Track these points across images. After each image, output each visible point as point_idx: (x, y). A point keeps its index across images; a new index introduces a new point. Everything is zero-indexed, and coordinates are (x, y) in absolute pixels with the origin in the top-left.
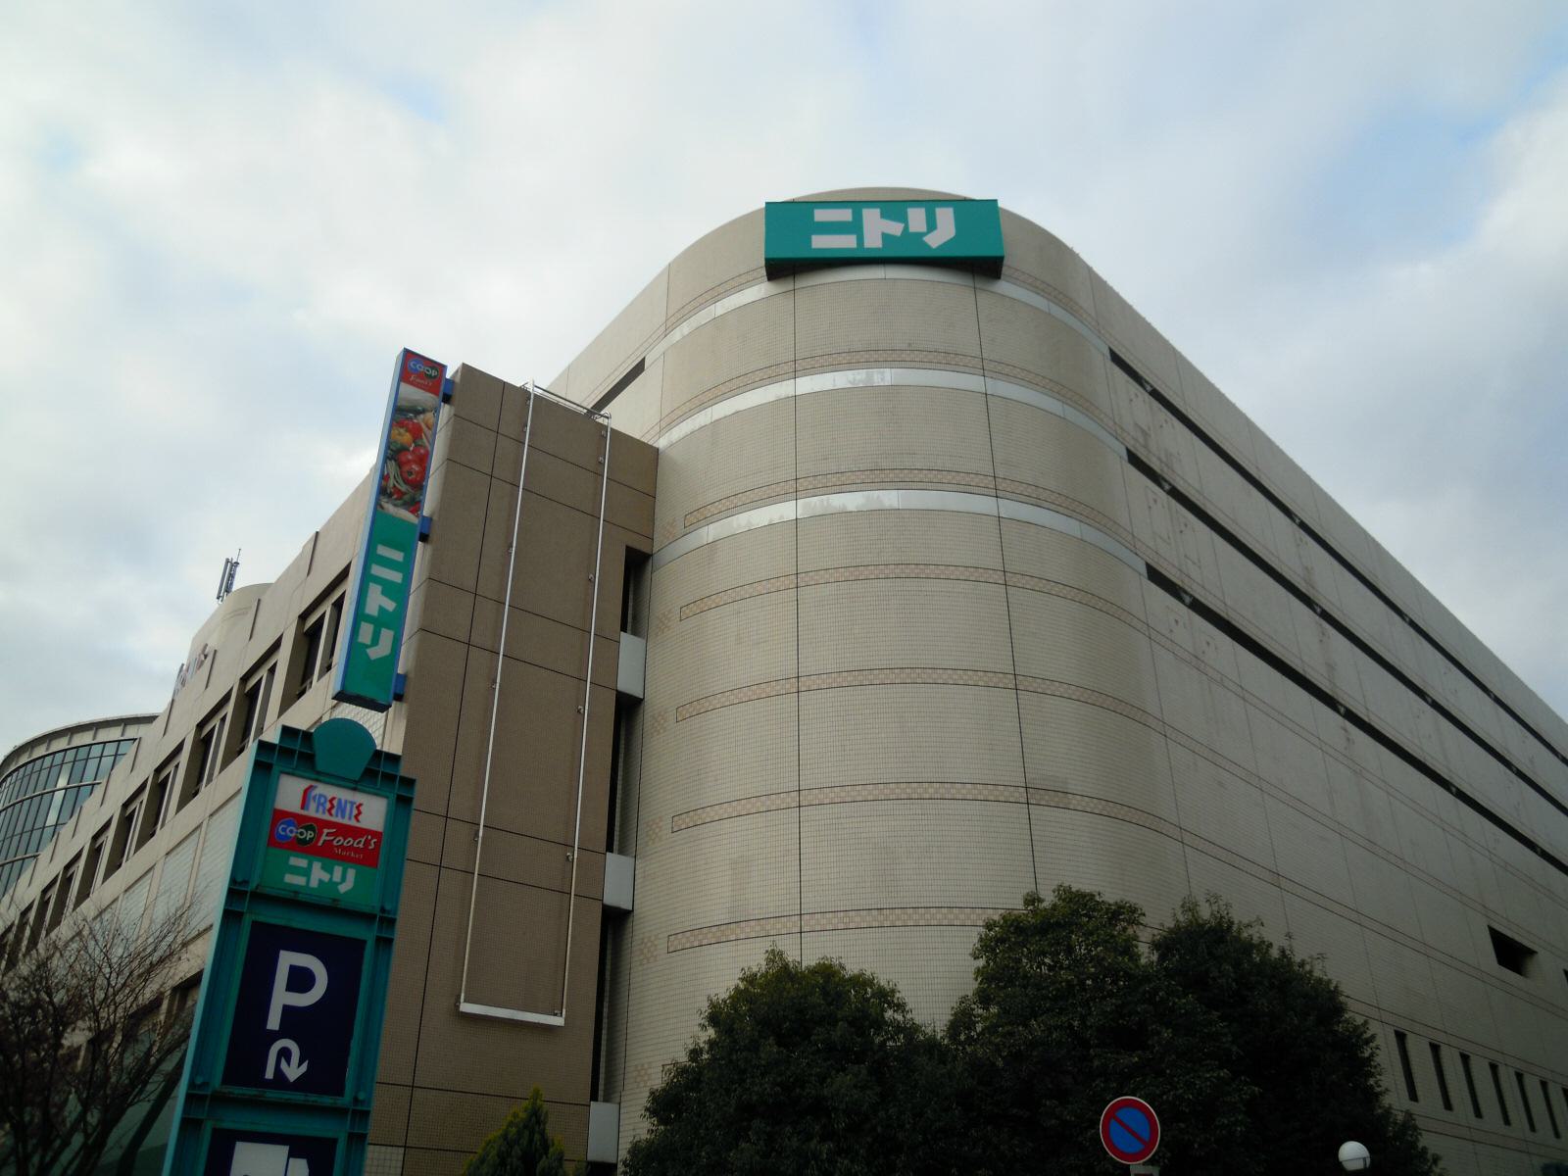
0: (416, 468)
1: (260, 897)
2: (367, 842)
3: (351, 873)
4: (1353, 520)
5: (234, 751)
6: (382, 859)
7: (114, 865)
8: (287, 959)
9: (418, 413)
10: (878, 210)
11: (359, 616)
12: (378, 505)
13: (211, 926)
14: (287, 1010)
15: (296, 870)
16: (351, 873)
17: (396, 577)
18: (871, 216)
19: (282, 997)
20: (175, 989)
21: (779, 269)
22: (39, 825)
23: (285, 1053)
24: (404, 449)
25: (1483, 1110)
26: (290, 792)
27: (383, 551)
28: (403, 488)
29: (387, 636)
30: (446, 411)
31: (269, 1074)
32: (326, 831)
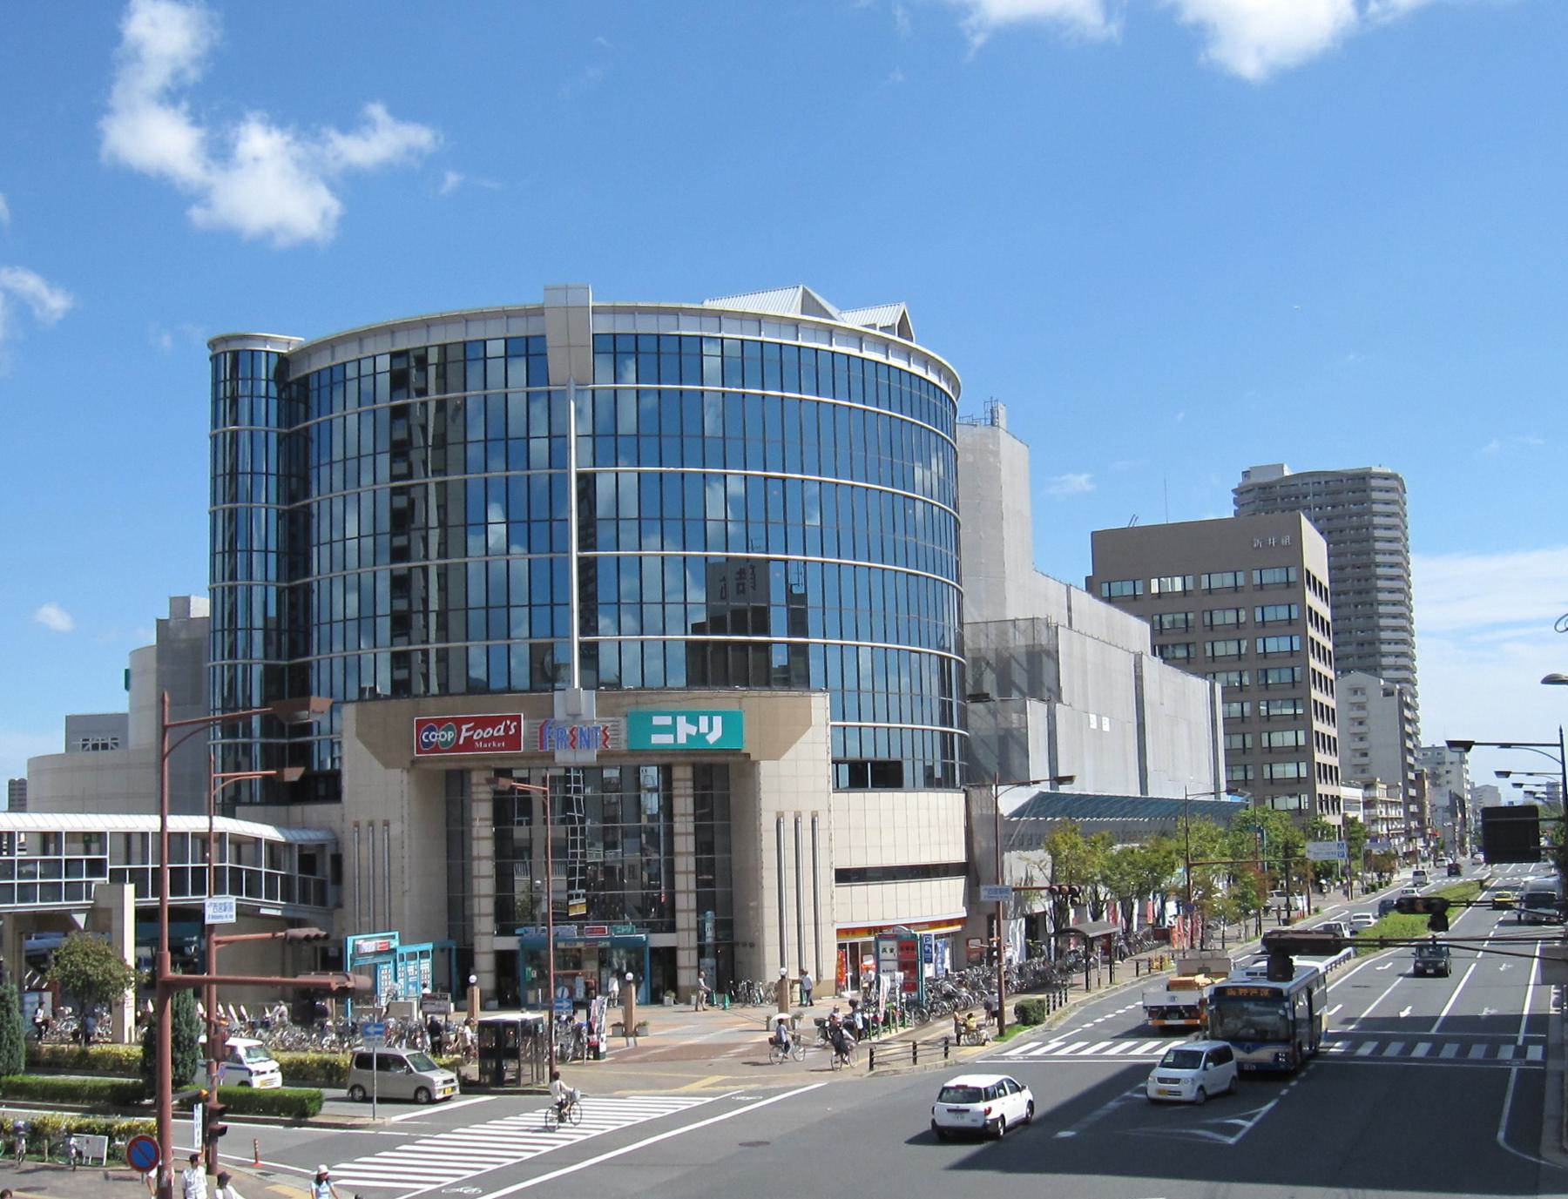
2: (507, 728)
3: (717, 721)
15: (662, 730)
25: (859, 890)
32: (464, 728)
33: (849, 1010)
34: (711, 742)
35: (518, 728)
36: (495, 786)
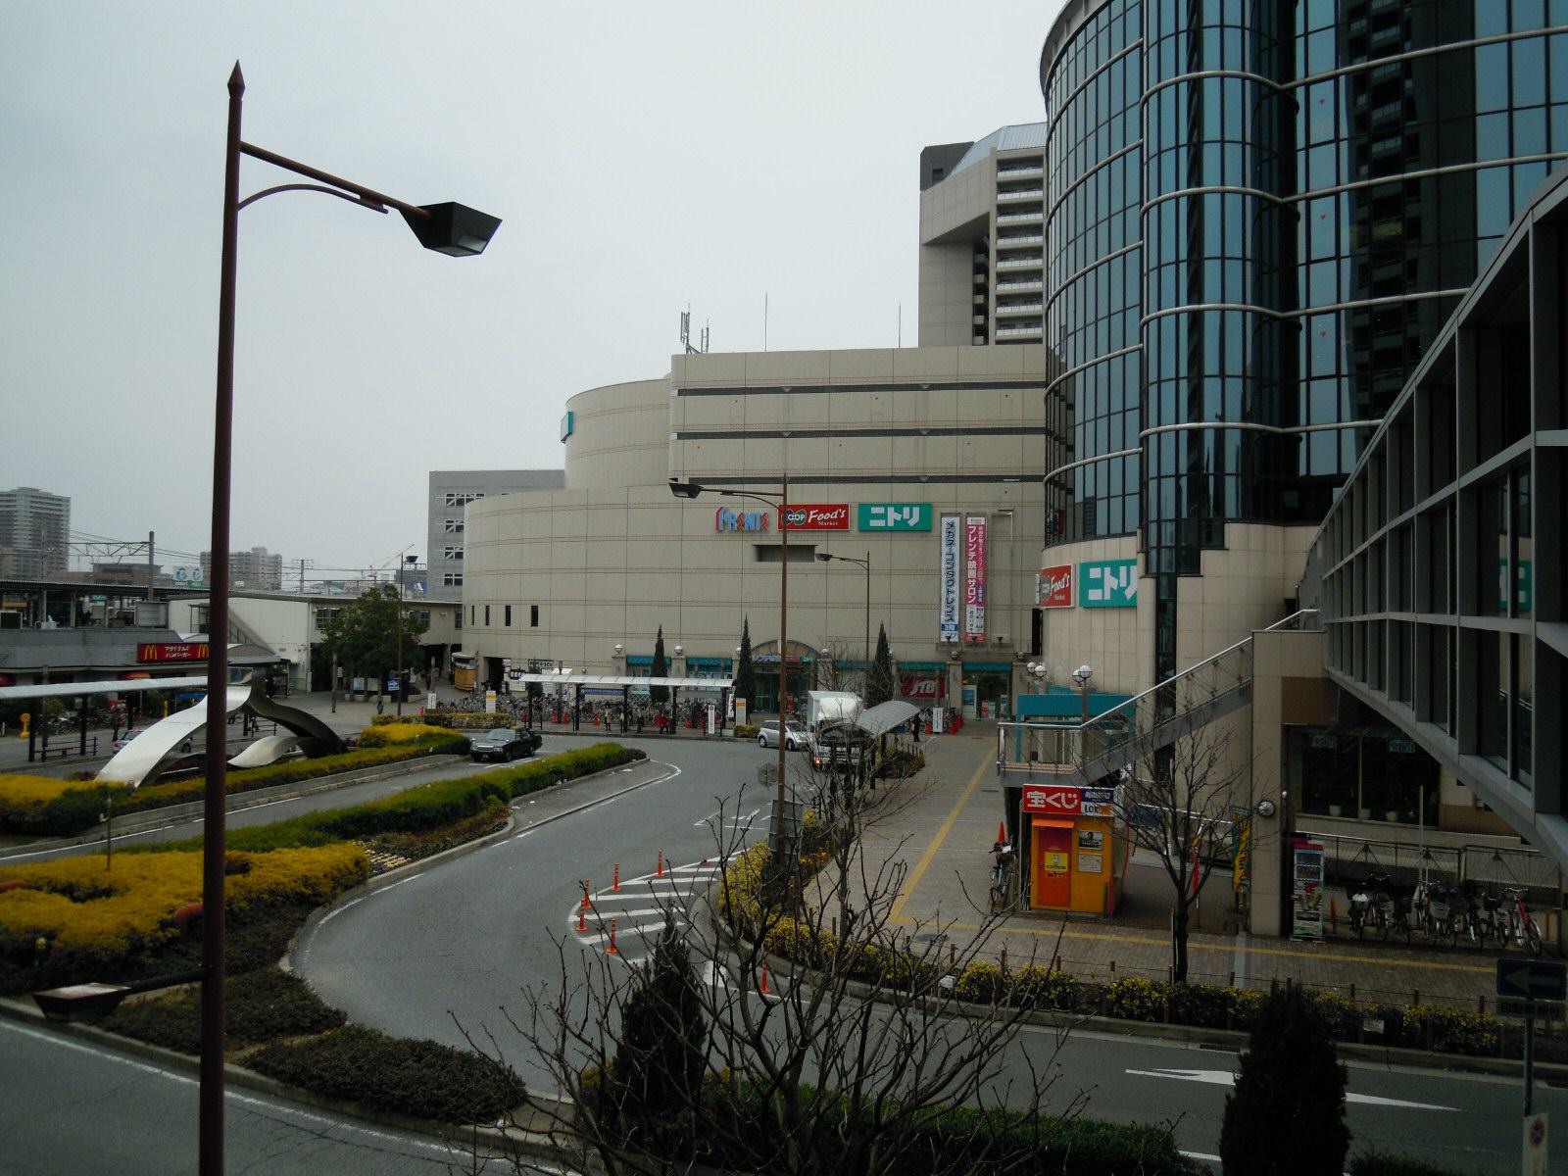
2: (839, 514)
3: (916, 510)
4: (486, 472)
6: (31, 764)
13: (1502, 236)
35: (846, 514)
36: (305, 677)
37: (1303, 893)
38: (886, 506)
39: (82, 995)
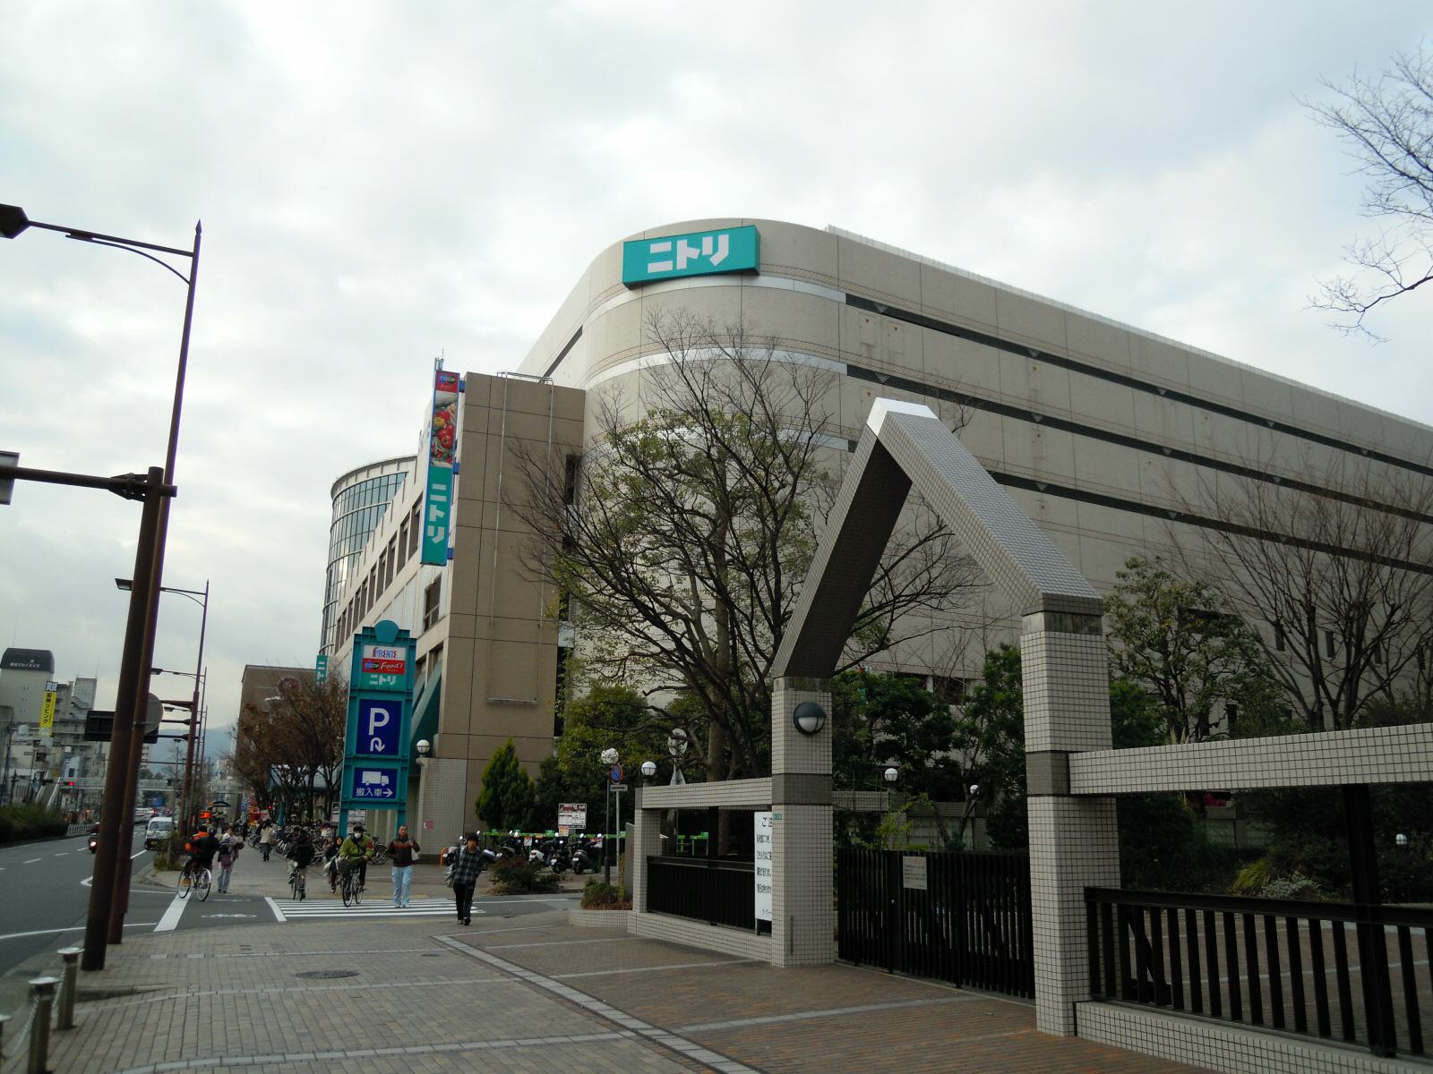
0: (448, 437)
1: (361, 690)
3: (724, 240)
5: (413, 549)
6: (406, 671)
7: (380, 593)
8: (374, 711)
9: (446, 405)
10: (686, 241)
11: (427, 523)
12: (430, 460)
14: (376, 728)
15: (373, 679)
16: (394, 677)
17: (443, 499)
18: (682, 244)
19: (373, 724)
20: (431, 651)
21: (632, 286)
22: (353, 538)
23: (376, 742)
24: (440, 429)
26: (368, 651)
27: (435, 487)
28: (442, 450)
29: (441, 530)
30: (461, 397)
31: (372, 749)
33: (1151, 558)
34: (715, 264)
37: (1255, 648)
38: (674, 239)
39: (427, 702)
